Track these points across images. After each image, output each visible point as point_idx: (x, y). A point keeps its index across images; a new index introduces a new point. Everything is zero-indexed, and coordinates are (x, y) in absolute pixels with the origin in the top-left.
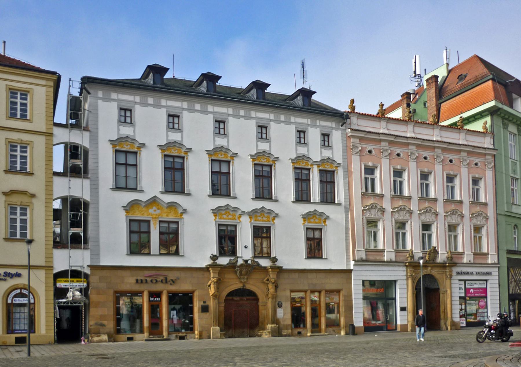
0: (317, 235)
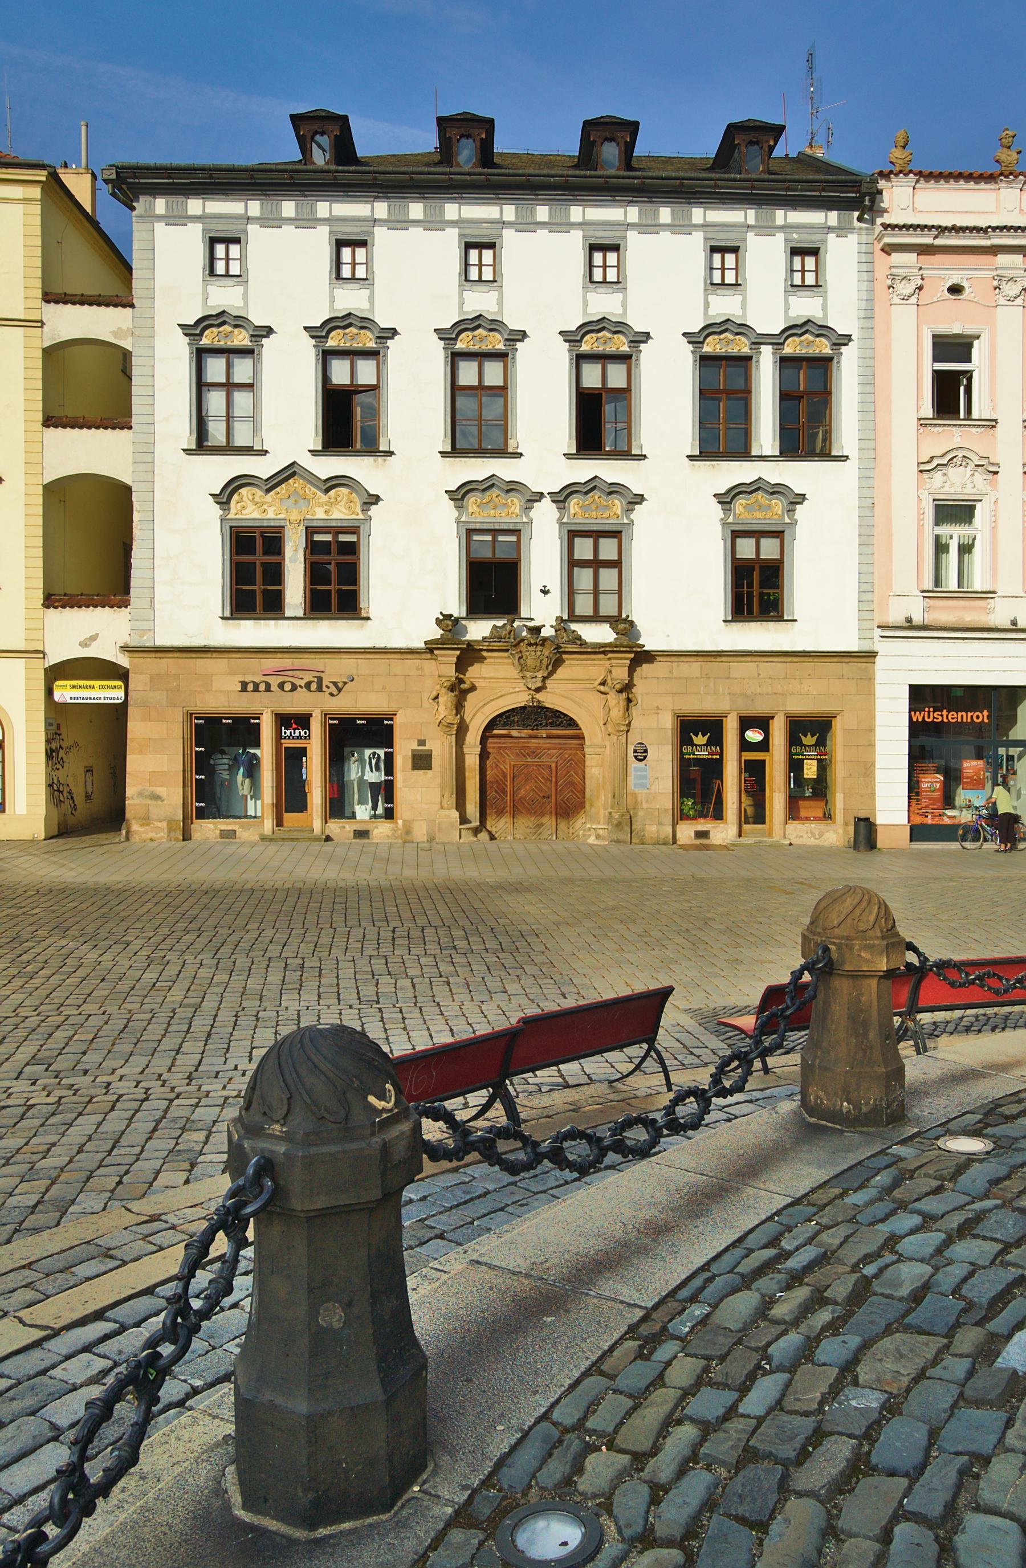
0: (769, 549)
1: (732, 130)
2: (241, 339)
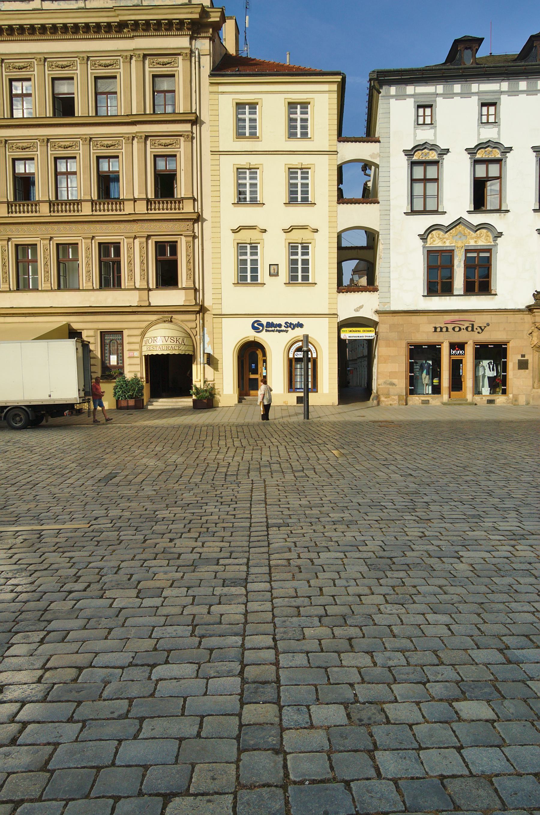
1: (457, 42)
2: (433, 156)
